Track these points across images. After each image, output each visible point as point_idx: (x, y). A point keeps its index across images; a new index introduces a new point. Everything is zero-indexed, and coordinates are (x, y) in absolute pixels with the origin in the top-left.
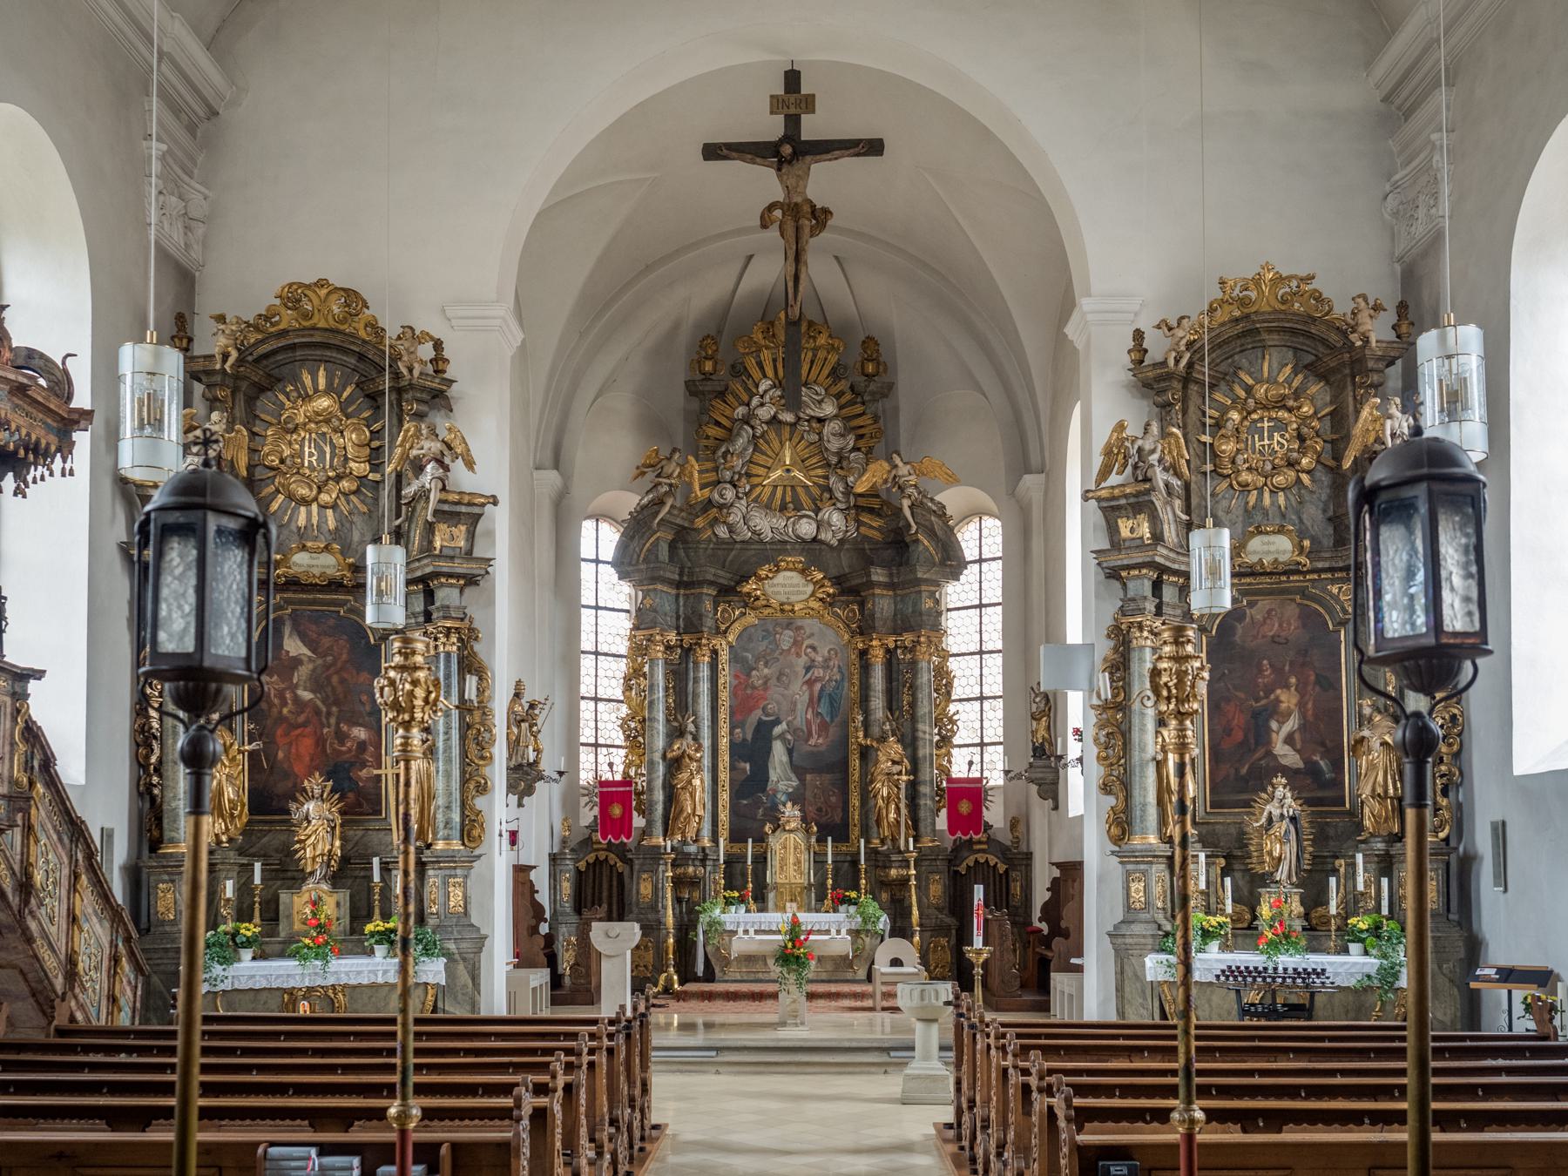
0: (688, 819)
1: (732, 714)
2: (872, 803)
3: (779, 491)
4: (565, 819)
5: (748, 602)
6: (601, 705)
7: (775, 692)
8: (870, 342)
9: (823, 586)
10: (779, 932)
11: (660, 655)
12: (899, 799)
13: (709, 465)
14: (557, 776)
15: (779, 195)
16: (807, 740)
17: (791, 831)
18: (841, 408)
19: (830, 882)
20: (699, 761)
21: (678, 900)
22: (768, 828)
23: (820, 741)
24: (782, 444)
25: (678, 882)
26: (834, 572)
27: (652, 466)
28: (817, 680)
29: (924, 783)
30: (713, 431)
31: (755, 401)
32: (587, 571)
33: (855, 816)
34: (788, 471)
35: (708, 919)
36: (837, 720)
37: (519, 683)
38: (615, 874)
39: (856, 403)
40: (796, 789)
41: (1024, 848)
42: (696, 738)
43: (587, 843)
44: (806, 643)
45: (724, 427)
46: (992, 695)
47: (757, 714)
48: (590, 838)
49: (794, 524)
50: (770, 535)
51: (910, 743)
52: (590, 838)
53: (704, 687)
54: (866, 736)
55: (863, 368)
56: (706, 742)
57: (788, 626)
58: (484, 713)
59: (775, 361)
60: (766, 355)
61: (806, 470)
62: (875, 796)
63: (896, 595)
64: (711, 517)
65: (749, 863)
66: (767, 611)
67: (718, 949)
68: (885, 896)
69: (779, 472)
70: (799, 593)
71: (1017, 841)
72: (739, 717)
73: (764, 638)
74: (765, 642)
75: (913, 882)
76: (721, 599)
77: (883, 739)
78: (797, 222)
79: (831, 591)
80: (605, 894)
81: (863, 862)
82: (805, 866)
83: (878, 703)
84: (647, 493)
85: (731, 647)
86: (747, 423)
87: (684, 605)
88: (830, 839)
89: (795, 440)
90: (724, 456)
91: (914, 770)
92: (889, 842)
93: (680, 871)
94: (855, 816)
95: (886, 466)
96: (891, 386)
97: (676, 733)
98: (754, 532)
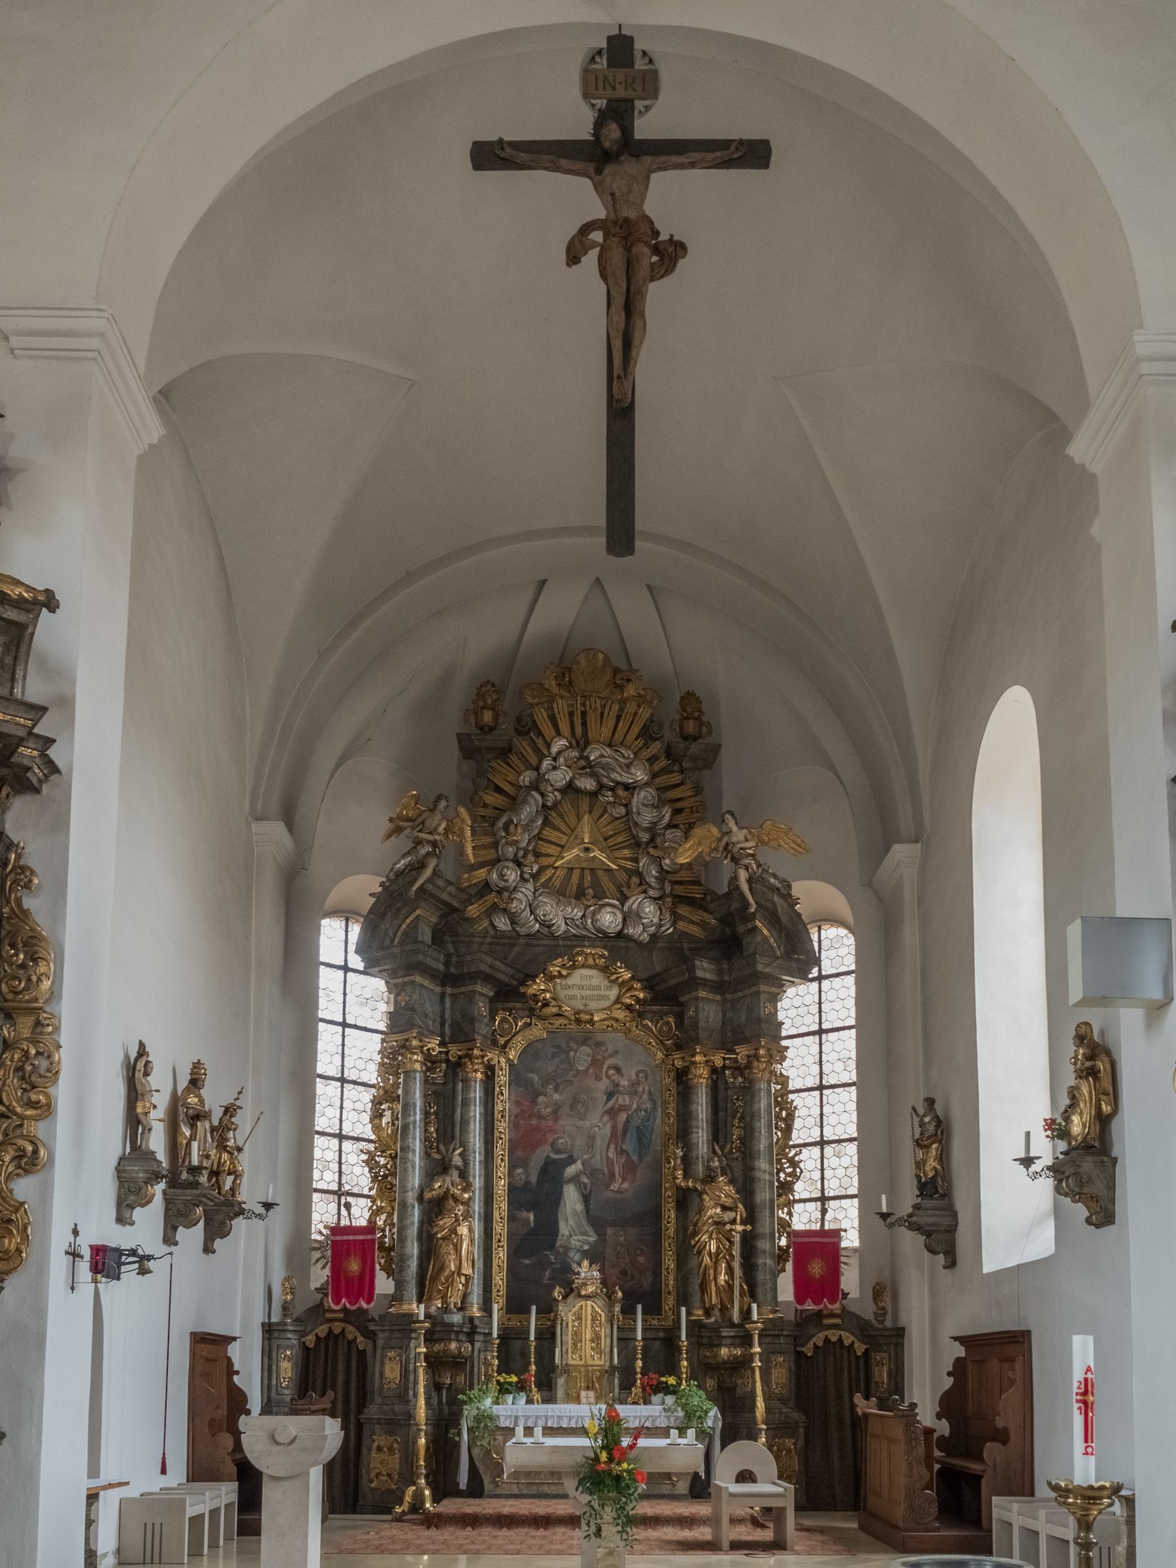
0: (450, 1282)
1: (512, 1149)
2: (694, 1262)
3: (576, 875)
4: (287, 1279)
5: (534, 1009)
6: (347, 1145)
7: (567, 1123)
8: (691, 703)
9: (631, 989)
10: (583, 1432)
11: (417, 1066)
12: (732, 1256)
13: (487, 840)
14: (262, 1211)
15: (599, 212)
16: (607, 1186)
17: (587, 1297)
18: (654, 776)
19: (639, 1363)
20: (467, 1203)
21: (435, 1386)
22: (557, 1293)
23: (625, 1185)
24: (579, 818)
25: (435, 1363)
26: (645, 975)
27: (411, 820)
28: (622, 1108)
29: (763, 1236)
30: (492, 799)
31: (546, 763)
32: (328, 980)
33: (670, 1281)
34: (587, 850)
35: (475, 1412)
36: (648, 1159)
37: (197, 1066)
38: (354, 1353)
39: (672, 772)
40: (594, 1246)
41: (888, 1323)
42: (464, 1174)
43: (318, 1310)
44: (609, 1062)
45: (506, 794)
46: (836, 1138)
47: (544, 1151)
48: (321, 1304)
49: (594, 913)
50: (563, 927)
51: (746, 1188)
52: (321, 1304)
53: (476, 1112)
54: (686, 1176)
55: (681, 727)
56: (478, 1182)
57: (585, 1041)
58: (38, 1023)
59: (571, 715)
60: (561, 707)
61: (611, 850)
62: (699, 1253)
63: (724, 1001)
64: (489, 904)
65: (532, 1338)
66: (559, 1022)
67: (488, 1452)
68: (710, 1383)
69: (575, 851)
70: (603, 998)
71: (881, 1314)
72: (519, 1153)
73: (553, 1055)
74: (557, 1060)
75: (757, 1363)
76: (499, 1005)
77: (710, 1178)
78: (628, 250)
79: (641, 995)
80: (341, 1378)
81: (684, 1338)
82: (605, 1343)
83: (701, 1136)
84: (404, 856)
85: (511, 1065)
86: (537, 790)
87: (452, 1007)
88: (639, 1307)
89: (596, 813)
90: (506, 828)
91: (750, 1218)
92: (718, 1313)
93: (438, 1347)
94: (670, 1281)
95: (715, 831)
96: (716, 749)
97: (438, 1167)
98: (543, 924)
